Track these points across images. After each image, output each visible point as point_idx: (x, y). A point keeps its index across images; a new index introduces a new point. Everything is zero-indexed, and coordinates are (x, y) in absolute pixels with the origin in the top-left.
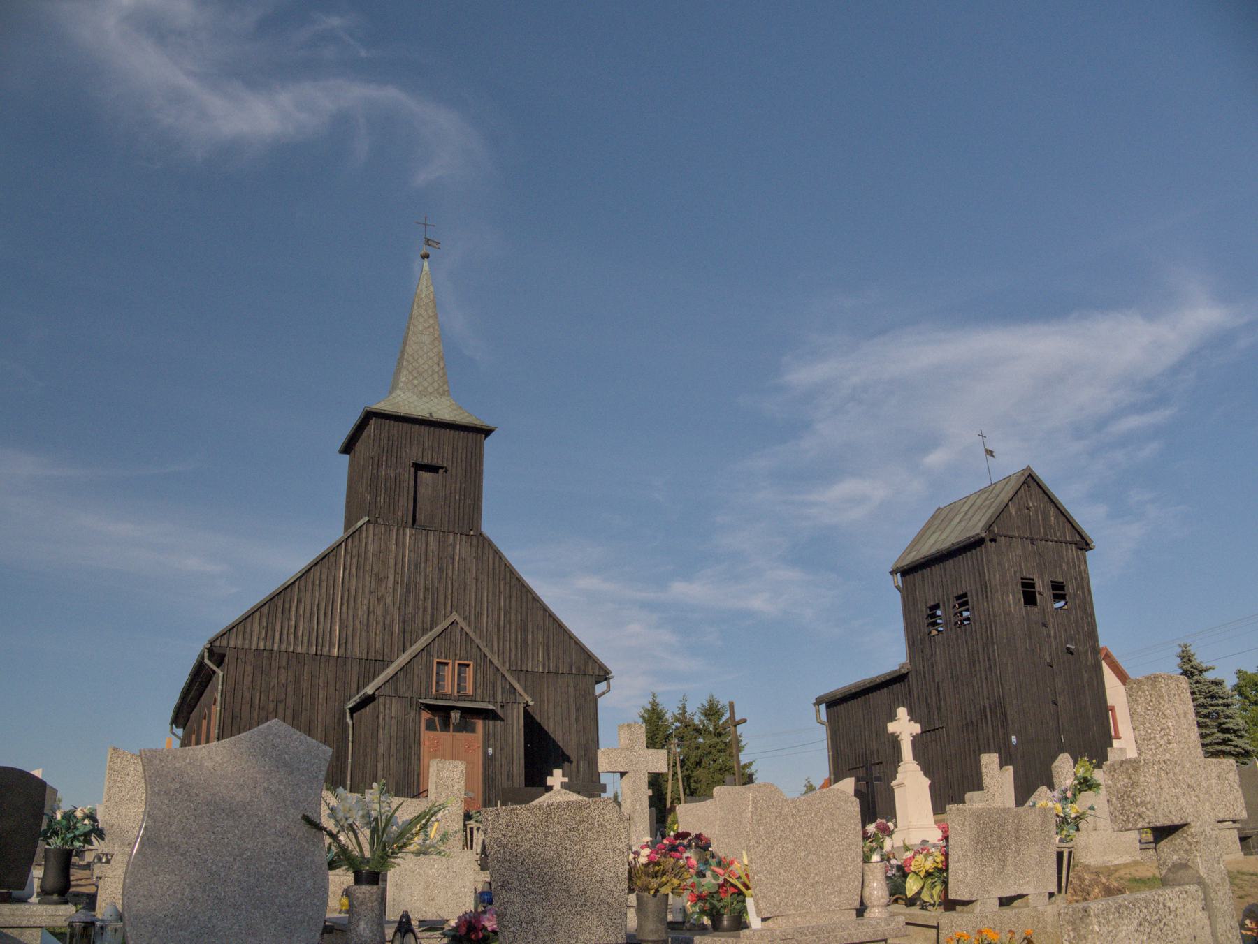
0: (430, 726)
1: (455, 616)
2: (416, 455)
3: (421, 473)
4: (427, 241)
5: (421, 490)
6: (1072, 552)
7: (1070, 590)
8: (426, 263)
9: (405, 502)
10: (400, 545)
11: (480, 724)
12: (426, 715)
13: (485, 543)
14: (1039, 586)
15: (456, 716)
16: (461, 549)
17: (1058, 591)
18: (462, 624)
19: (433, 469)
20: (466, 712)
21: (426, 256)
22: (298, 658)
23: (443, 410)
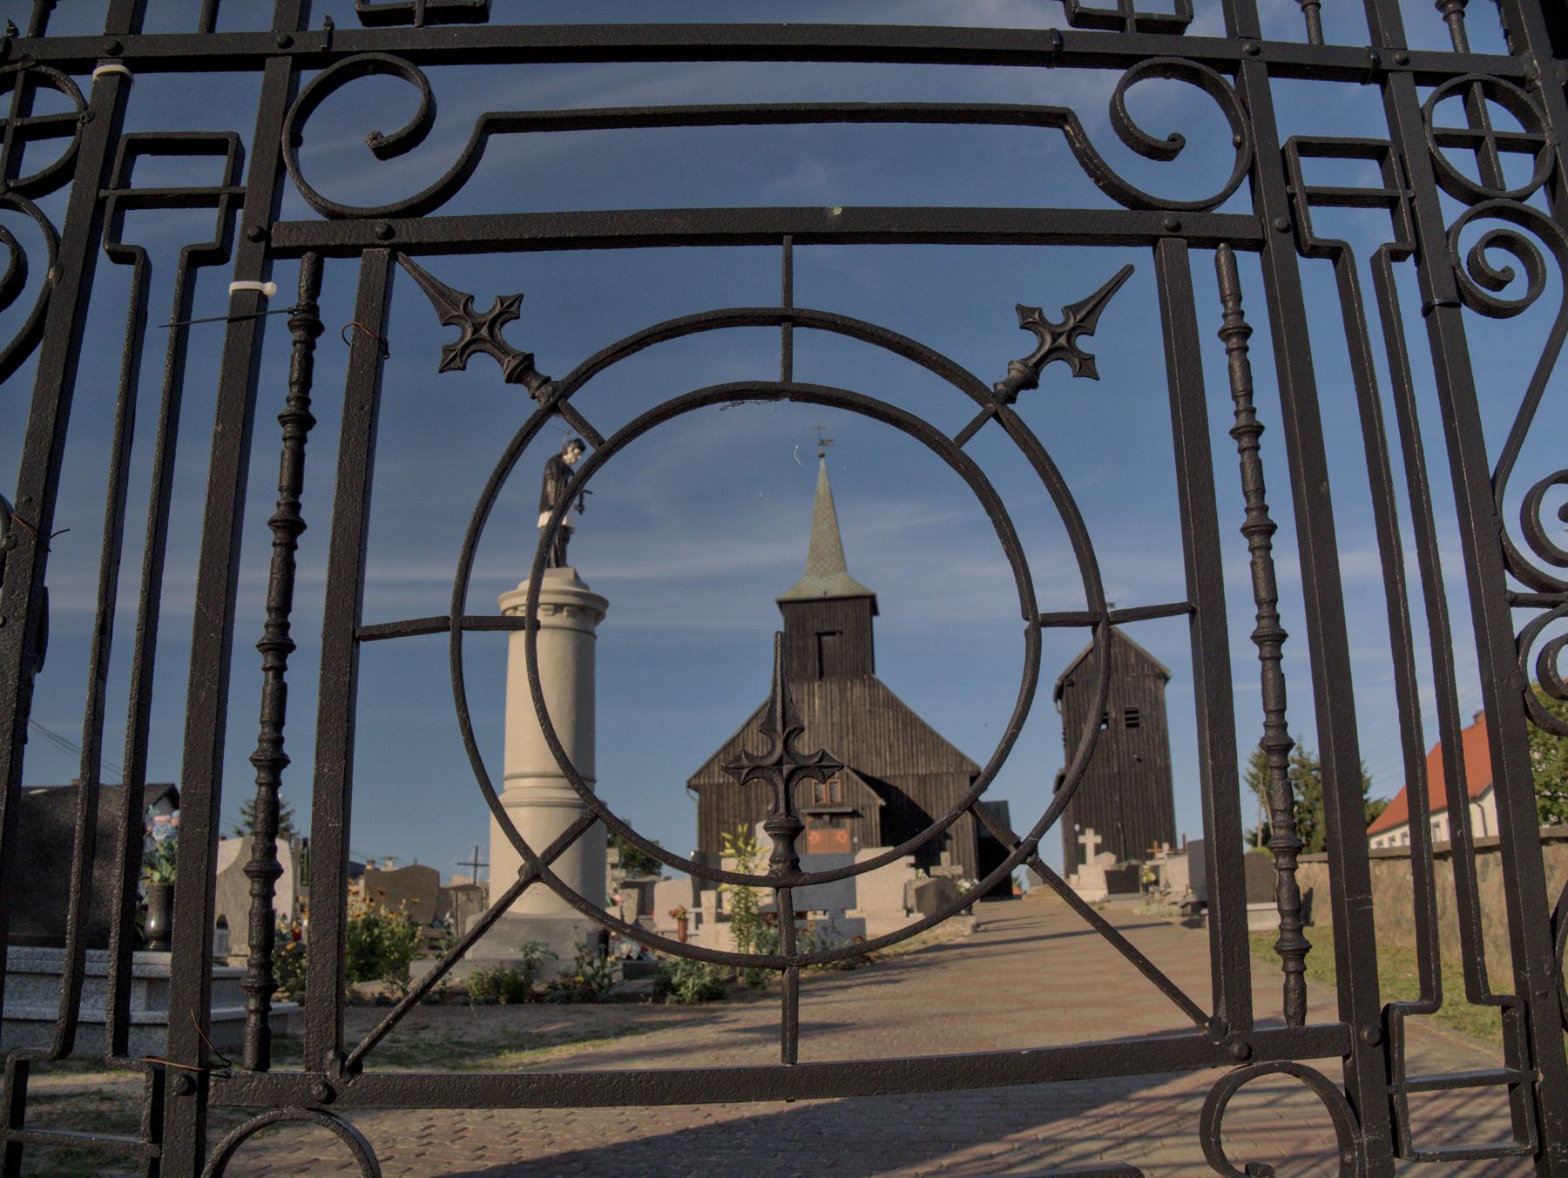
0: (816, 828)
2: (819, 627)
3: (825, 638)
5: (825, 651)
7: (1145, 712)
8: (822, 462)
9: (813, 664)
10: (811, 695)
11: (848, 821)
13: (875, 684)
15: (827, 818)
16: (857, 691)
19: (833, 634)
20: (833, 815)
21: (822, 456)
23: (836, 586)
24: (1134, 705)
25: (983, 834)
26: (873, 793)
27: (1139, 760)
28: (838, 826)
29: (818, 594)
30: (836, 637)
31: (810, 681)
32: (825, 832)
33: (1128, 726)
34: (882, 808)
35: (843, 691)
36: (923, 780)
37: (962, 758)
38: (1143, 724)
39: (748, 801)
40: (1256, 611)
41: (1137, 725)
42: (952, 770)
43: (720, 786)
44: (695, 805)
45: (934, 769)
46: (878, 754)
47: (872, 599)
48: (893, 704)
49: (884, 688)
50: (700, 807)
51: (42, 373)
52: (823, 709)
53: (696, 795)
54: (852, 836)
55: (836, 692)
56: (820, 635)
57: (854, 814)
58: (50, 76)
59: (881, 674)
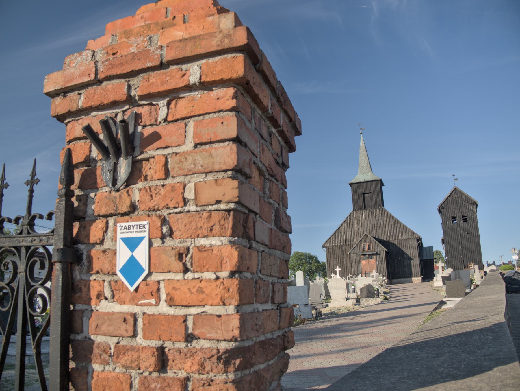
0: (364, 259)
1: (366, 233)
3: (365, 195)
4: (361, 129)
5: (366, 199)
6: (470, 206)
7: (469, 216)
9: (362, 204)
10: (362, 214)
11: (375, 256)
12: (362, 256)
14: (458, 218)
15: (367, 256)
16: (377, 212)
17: (465, 219)
18: (367, 234)
19: (368, 193)
20: (369, 255)
22: (342, 246)
24: (466, 214)
25: (425, 258)
26: (383, 247)
27: (468, 233)
28: (371, 258)
29: (362, 180)
30: (369, 194)
31: (361, 209)
32: (367, 260)
33: (463, 222)
34: (386, 252)
35: (372, 213)
36: (401, 241)
37: (414, 233)
38: (469, 221)
39: (342, 251)
40: (288, 174)
41: (467, 221)
42: (410, 237)
43: (333, 246)
44: (325, 253)
45: (404, 237)
46: (385, 233)
47: (381, 181)
48: (389, 216)
49: (386, 211)
50: (327, 254)
51: (94, 145)
52: (366, 219)
53: (325, 249)
54: (376, 261)
55: (370, 213)
56: (364, 194)
57: (377, 254)
58: (33, 261)
59: (389, 207)
